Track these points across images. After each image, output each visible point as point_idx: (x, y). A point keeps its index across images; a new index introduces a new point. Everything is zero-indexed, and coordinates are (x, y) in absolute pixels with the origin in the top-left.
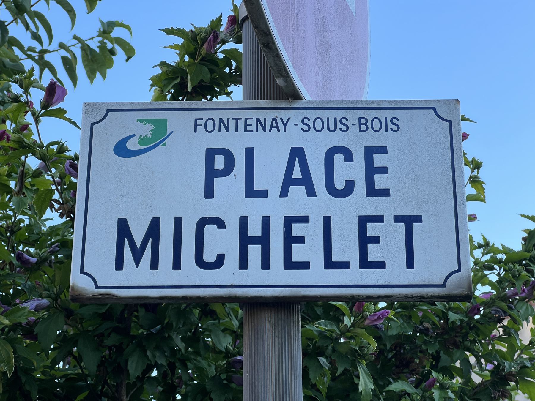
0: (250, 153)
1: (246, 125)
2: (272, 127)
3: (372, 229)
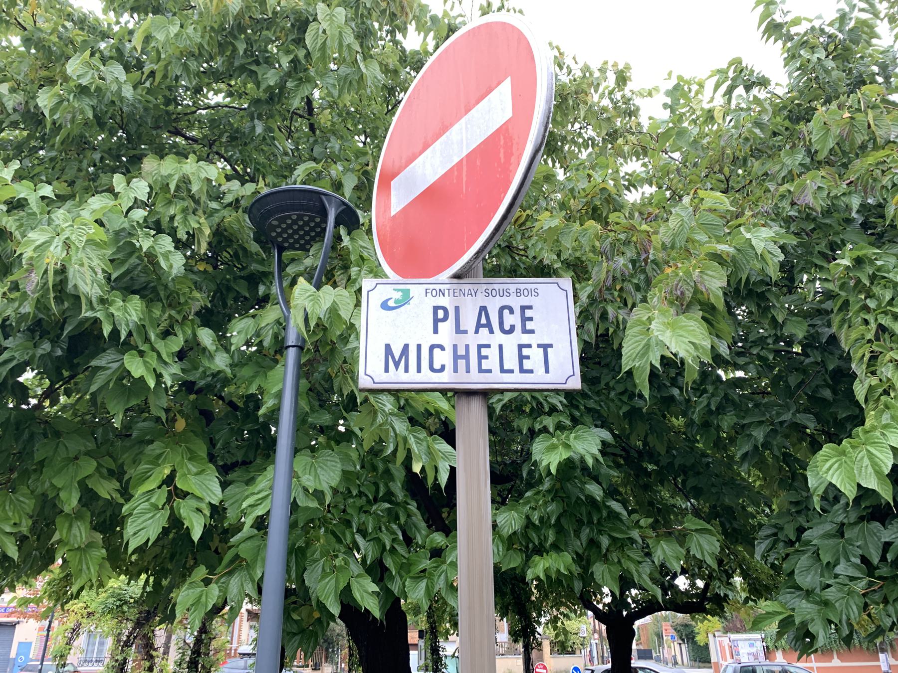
0: (457, 309)
1: (481, 358)
2: (479, 326)
3: (525, 352)
